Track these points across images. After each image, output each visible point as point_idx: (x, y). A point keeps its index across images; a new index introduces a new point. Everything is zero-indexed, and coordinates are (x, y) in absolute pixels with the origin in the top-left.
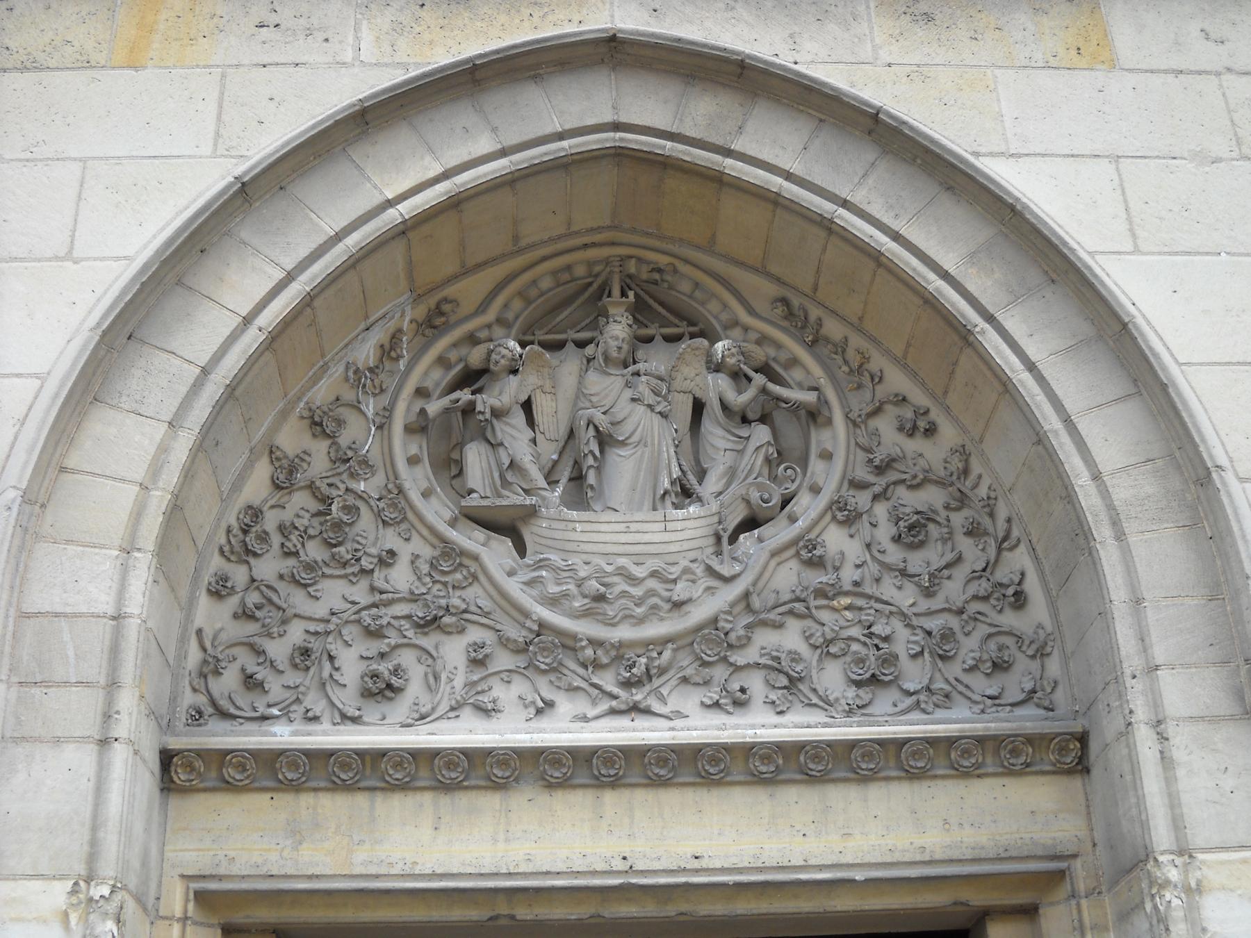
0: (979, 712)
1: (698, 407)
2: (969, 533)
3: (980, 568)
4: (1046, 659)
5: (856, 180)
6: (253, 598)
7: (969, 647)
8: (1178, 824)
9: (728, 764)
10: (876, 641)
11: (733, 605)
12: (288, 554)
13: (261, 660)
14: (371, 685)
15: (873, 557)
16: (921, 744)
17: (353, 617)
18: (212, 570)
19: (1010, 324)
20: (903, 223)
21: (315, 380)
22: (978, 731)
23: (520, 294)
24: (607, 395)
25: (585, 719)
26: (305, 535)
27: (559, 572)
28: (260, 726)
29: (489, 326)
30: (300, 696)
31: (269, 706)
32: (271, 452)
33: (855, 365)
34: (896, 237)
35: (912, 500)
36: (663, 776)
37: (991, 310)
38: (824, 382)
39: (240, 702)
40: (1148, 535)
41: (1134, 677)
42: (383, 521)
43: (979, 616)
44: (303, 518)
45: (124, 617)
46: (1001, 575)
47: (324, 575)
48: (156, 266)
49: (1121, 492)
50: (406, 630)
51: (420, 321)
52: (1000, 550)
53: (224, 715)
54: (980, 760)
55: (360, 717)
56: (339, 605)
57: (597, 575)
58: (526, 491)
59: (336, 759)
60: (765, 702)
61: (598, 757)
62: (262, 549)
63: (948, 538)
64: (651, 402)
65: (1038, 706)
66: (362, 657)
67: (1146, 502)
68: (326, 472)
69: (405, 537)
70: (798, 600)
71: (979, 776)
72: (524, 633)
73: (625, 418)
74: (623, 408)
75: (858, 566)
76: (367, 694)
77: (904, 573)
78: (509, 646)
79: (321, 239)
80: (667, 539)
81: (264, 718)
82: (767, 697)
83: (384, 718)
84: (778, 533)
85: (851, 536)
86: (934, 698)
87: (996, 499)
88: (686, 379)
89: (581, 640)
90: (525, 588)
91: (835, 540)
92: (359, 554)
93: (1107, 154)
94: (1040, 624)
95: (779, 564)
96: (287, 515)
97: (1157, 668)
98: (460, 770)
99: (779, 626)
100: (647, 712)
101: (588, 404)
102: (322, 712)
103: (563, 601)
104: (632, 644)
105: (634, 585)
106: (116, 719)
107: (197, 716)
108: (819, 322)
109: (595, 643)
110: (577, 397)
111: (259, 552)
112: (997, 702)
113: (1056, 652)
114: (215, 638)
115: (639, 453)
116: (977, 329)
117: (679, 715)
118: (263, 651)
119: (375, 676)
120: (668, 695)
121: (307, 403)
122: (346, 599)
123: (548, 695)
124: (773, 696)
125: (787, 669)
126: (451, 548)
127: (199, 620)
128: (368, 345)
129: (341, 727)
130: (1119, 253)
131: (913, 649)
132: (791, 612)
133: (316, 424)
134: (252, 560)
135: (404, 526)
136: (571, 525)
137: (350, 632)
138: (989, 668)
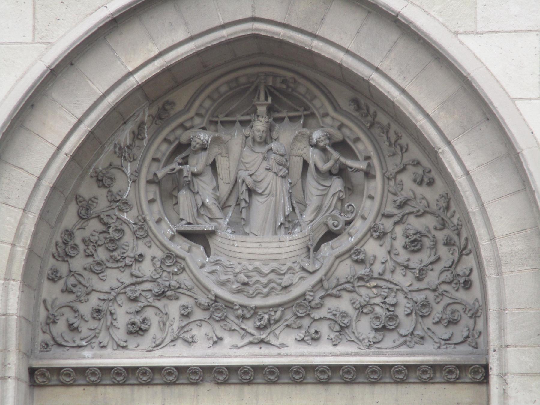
0: (437, 348)
1: (306, 164)
2: (446, 244)
3: (448, 266)
4: (477, 319)
5: (385, 54)
6: (72, 281)
7: (437, 310)
9: (304, 374)
10: (388, 307)
11: (313, 287)
12: (88, 256)
13: (76, 315)
14: (131, 329)
15: (391, 258)
16: (401, 367)
17: (122, 291)
18: (49, 267)
19: (457, 148)
20: (407, 83)
21: (99, 155)
22: (431, 362)
23: (209, 97)
24: (254, 165)
25: (237, 347)
26: (96, 245)
27: (227, 269)
28: (77, 351)
29: (192, 118)
30: (97, 335)
31: (82, 340)
32: (76, 199)
33: (393, 140)
34: (403, 91)
36: (272, 380)
37: (449, 138)
38: (373, 154)
39: (67, 338)
40: (515, 274)
41: (495, 351)
42: (137, 238)
43: (444, 293)
44: (95, 236)
45: (9, 316)
46: (461, 269)
47: (107, 267)
48: (10, 122)
49: (504, 248)
50: (149, 298)
51: (154, 115)
52: (461, 255)
53: (60, 345)
54: (432, 376)
55: (126, 346)
56: (116, 284)
57: (244, 271)
58: (211, 219)
59: (114, 371)
60: (328, 339)
61: (241, 371)
62: (74, 253)
63: (434, 246)
64: (276, 171)
65: (469, 345)
66: (127, 313)
67: (517, 254)
68: (106, 208)
69: (148, 245)
70: (348, 282)
71: (433, 383)
72: (208, 301)
73: (262, 180)
74: (261, 173)
75: (383, 263)
76: (130, 333)
77: (407, 267)
78: (201, 307)
79: (95, 98)
80: (280, 252)
81: (79, 347)
82: (329, 336)
83: (138, 346)
85: (381, 246)
86: (415, 339)
87: (462, 225)
88: (299, 149)
89: (236, 305)
90: (209, 275)
92: (125, 255)
93: (536, 29)
94: (477, 299)
95: (340, 262)
96: (86, 234)
97: (508, 346)
98: (174, 376)
99: (338, 297)
100: (268, 343)
101: (244, 168)
102: (108, 343)
103: (228, 284)
104: (262, 308)
105: (263, 277)
106: (9, 367)
107: (46, 346)
108: (375, 115)
110: (238, 164)
111: (73, 255)
112: (447, 342)
113: (482, 316)
114: (53, 303)
115: (269, 200)
116: (440, 151)
117: (283, 345)
118: (78, 310)
119: (133, 324)
120: (279, 334)
121: (94, 169)
122: (119, 281)
123: (220, 334)
124: (332, 336)
125: (339, 322)
126: (171, 254)
127: (44, 295)
128: (126, 133)
129: (117, 352)
130: (530, 99)
131: (407, 311)
132: (344, 289)
133: (100, 180)
134: (70, 260)
135: (148, 239)
136: (232, 243)
137: (122, 299)
138: (446, 323)
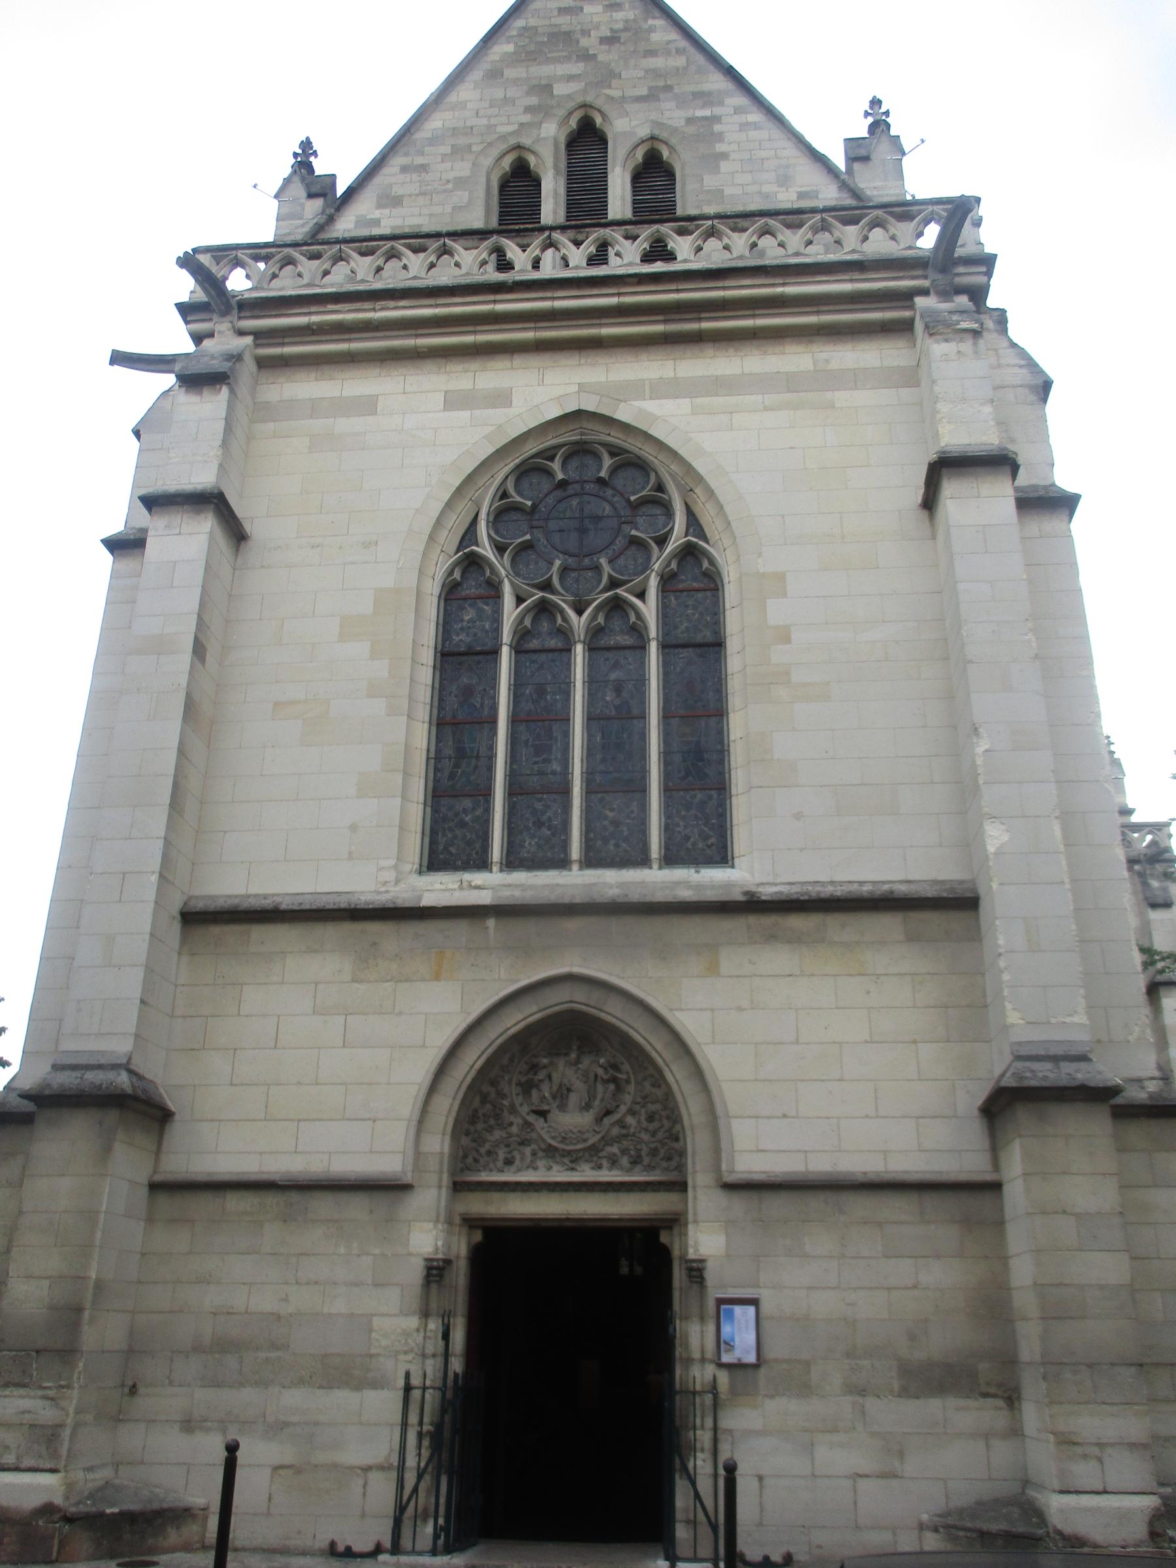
1: (596, 1076)
7: (662, 1153)
8: (695, 1214)
35: (652, 1107)
63: (660, 1120)
84: (616, 1117)
91: (630, 1120)
99: (612, 1145)
104: (573, 1151)
107: (462, 1170)
109: (563, 1150)
117: (583, 1171)
137: (502, 1146)
